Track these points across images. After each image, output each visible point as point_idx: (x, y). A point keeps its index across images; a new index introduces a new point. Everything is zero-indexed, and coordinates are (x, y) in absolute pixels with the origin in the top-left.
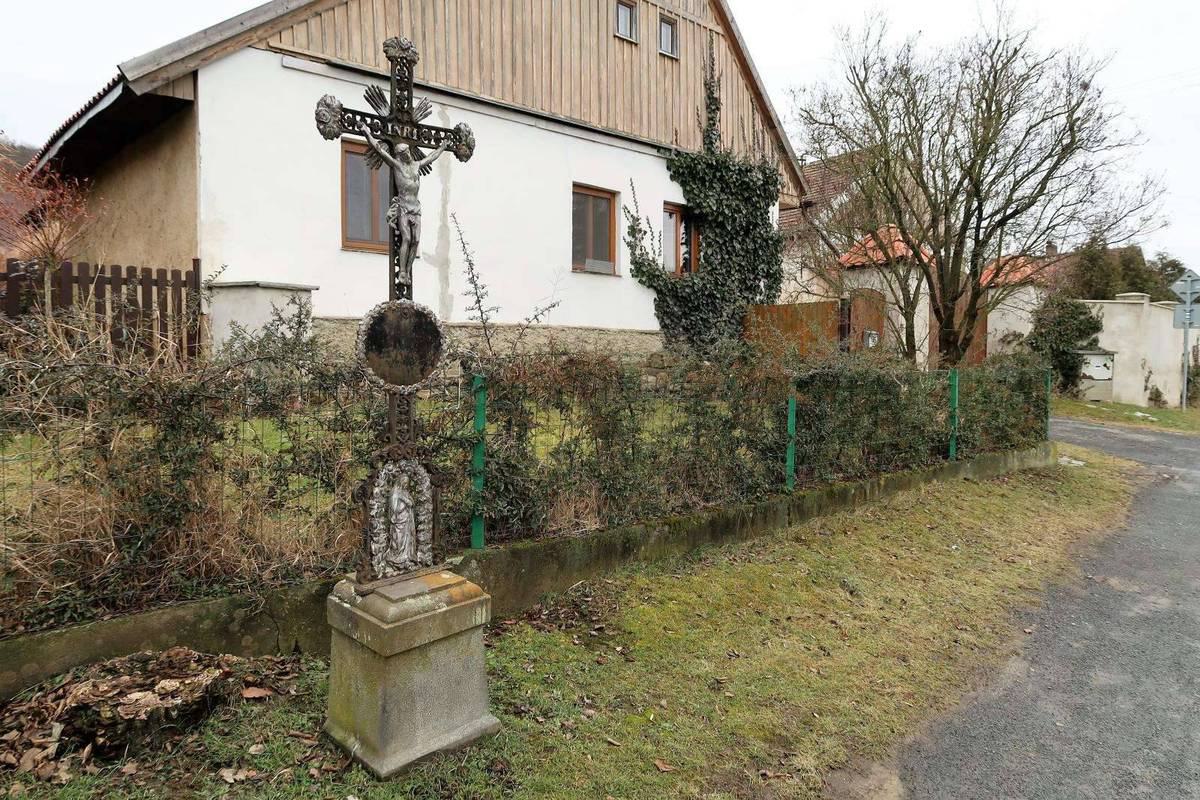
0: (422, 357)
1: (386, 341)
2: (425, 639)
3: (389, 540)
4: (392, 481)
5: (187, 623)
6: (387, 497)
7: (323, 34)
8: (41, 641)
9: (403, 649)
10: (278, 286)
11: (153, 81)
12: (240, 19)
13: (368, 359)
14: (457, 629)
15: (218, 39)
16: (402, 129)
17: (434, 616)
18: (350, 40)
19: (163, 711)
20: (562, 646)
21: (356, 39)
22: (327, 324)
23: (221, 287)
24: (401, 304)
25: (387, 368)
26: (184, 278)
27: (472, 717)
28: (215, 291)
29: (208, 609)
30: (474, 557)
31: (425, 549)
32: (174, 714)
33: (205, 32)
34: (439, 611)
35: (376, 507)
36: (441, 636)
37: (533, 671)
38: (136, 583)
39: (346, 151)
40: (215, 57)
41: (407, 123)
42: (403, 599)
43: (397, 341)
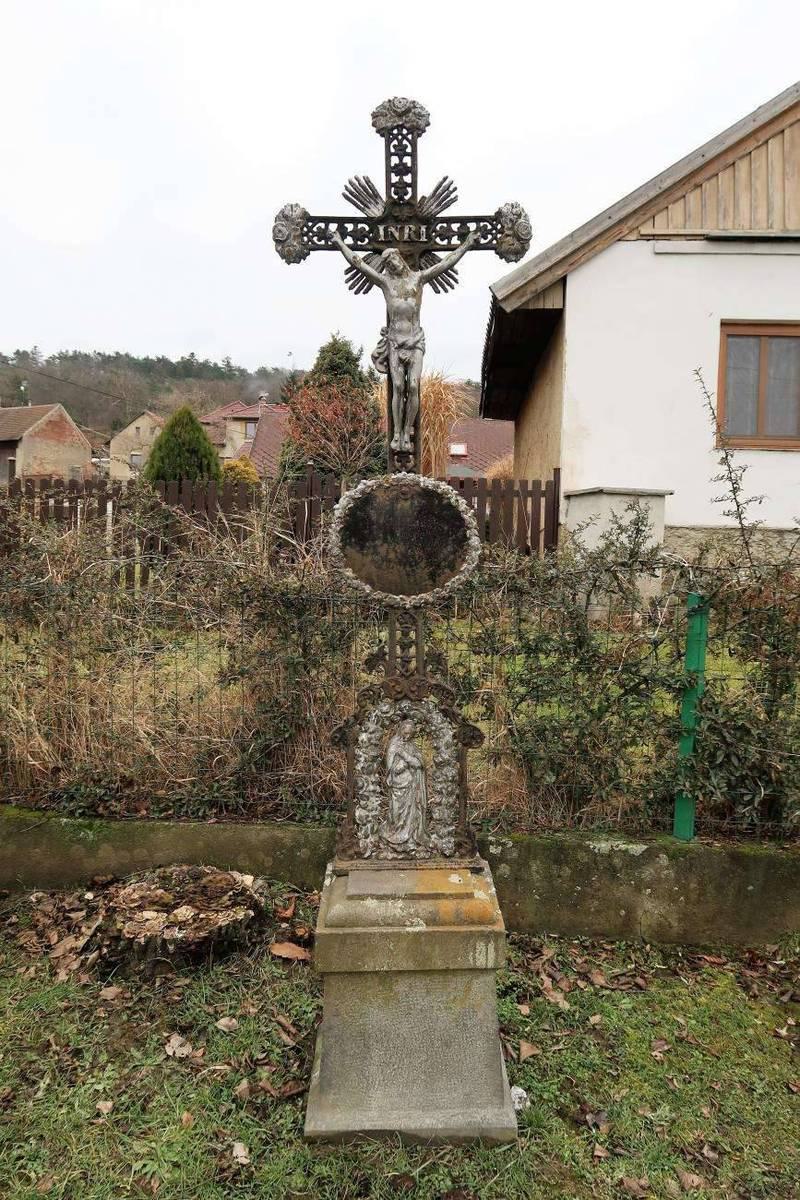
0: (431, 557)
1: (371, 532)
2: (383, 964)
3: (383, 805)
4: (389, 725)
5: (283, 846)
6: (381, 746)
7: (703, 206)
8: (152, 830)
9: (344, 968)
10: (623, 491)
11: (522, 296)
12: (607, 214)
13: (345, 556)
14: (439, 964)
15: (585, 239)
16: (402, 230)
17: (398, 935)
18: (736, 206)
19: (159, 941)
20: (751, 1031)
21: (744, 203)
22: (693, 533)
23: (576, 496)
24: (398, 480)
25: (373, 569)
26: (543, 488)
27: (468, 1102)
28: (572, 500)
29: (307, 837)
30: (665, 850)
31: (445, 831)
32: (171, 948)
33: (572, 235)
34: (408, 929)
35: (362, 759)
36: (411, 966)
37: (660, 1056)
38: (256, 792)
39: (729, 336)
40: (583, 260)
41: (409, 220)
42: (361, 897)
43: (389, 532)
